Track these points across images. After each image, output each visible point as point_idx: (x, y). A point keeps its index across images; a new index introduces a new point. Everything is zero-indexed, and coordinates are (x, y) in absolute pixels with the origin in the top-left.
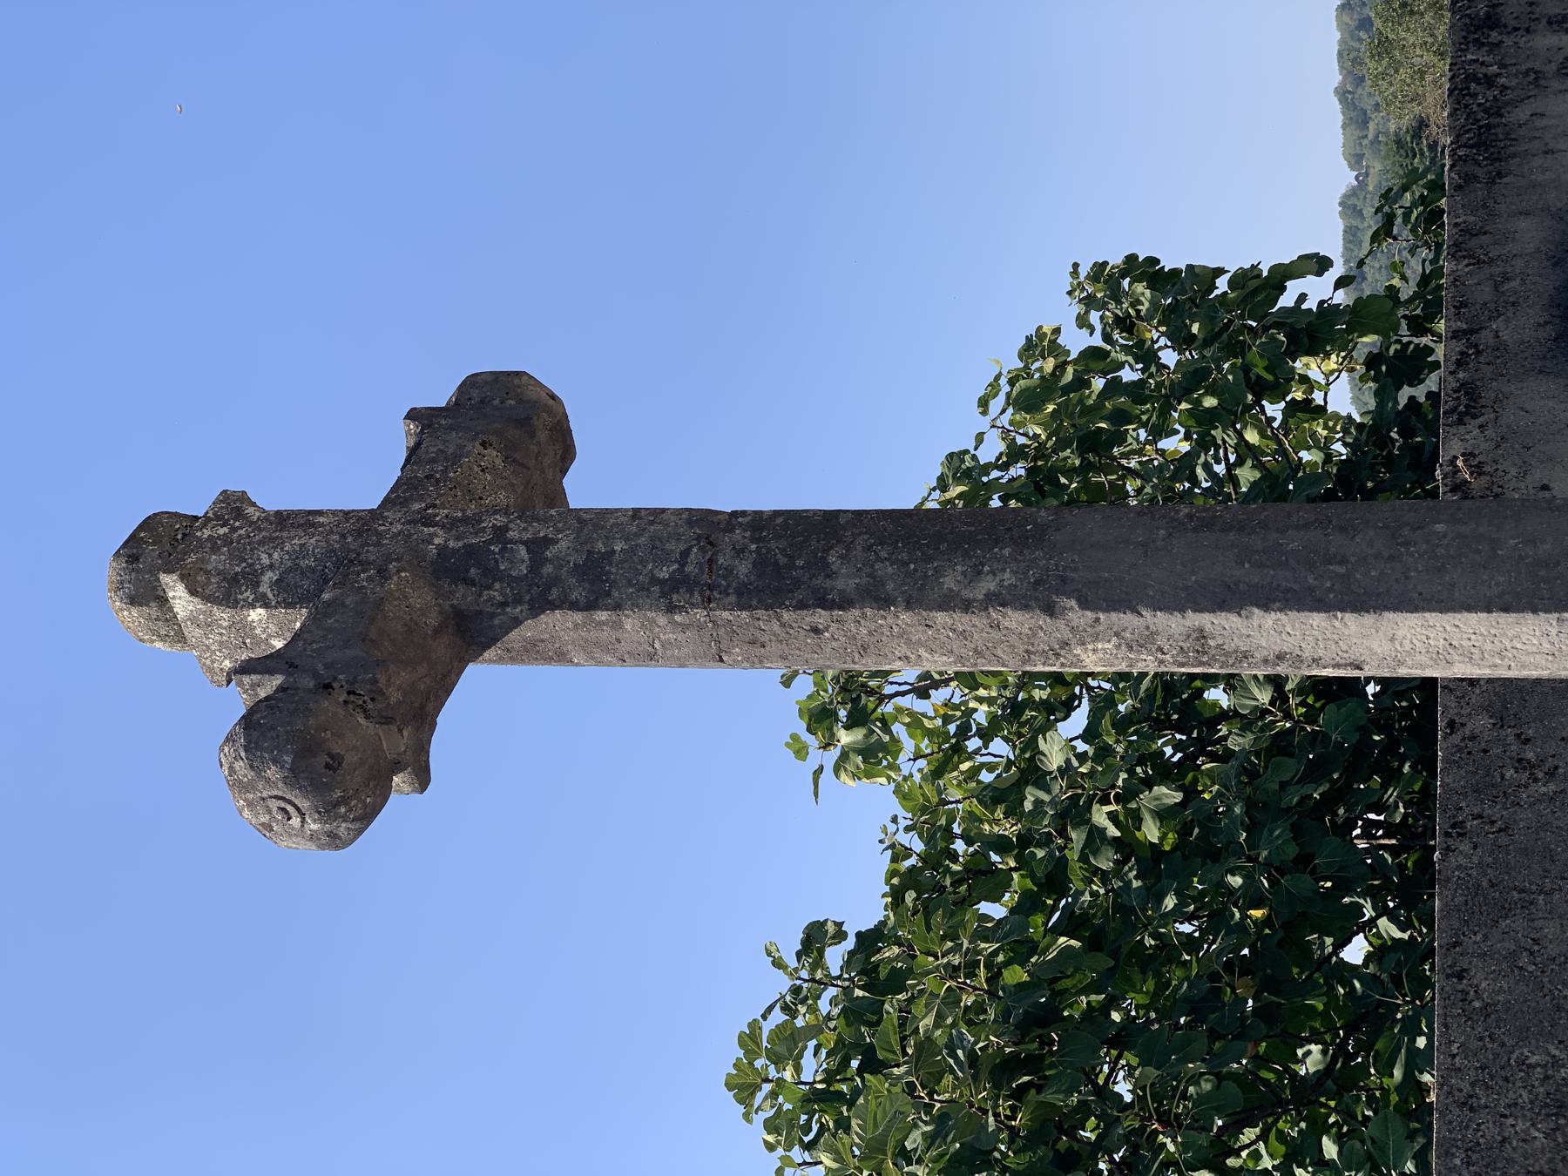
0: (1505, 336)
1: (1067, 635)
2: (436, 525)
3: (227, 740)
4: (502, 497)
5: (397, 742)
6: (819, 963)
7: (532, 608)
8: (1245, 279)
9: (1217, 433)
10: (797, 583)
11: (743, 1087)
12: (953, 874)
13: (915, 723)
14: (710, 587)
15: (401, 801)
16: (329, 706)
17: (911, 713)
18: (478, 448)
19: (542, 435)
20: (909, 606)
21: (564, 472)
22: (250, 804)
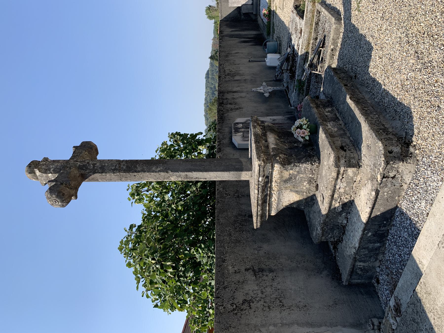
0: (224, 142)
1: (169, 176)
2: (78, 162)
3: (46, 191)
4: (88, 158)
5: (73, 192)
6: (132, 230)
7: (93, 173)
8: (192, 135)
9: (188, 156)
10: (132, 169)
11: (120, 249)
12: (152, 217)
13: (146, 195)
14: (120, 170)
15: (73, 201)
16: (63, 186)
17: (146, 194)
18: (84, 151)
19: (94, 150)
20: (148, 172)
21: (97, 156)
22: (50, 201)
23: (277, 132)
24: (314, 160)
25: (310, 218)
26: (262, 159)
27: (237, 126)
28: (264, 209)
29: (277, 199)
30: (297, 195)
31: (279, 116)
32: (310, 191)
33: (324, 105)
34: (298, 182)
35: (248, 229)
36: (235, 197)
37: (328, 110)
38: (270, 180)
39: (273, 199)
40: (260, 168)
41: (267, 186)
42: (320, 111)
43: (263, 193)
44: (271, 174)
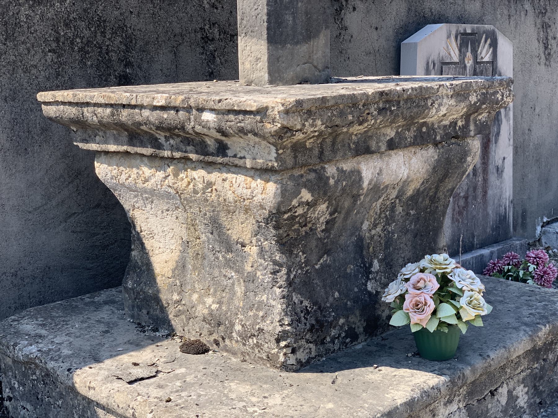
23: (437, 188)
24: (300, 348)
25: (98, 306)
26: (296, 122)
27: (486, 42)
28: (108, 132)
29: (148, 185)
30: (172, 265)
31: (514, 187)
32: (183, 317)
33: (541, 378)
34: (216, 273)
35: (70, 71)
36: (207, 27)
37: (520, 394)
38: (211, 159)
39: (147, 171)
40: (250, 113)
41: (189, 148)
42: (518, 364)
43: (158, 128)
44: (236, 166)
